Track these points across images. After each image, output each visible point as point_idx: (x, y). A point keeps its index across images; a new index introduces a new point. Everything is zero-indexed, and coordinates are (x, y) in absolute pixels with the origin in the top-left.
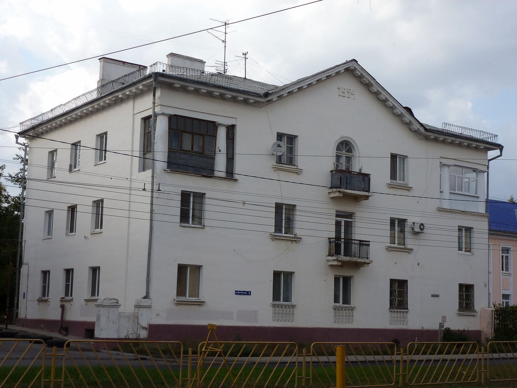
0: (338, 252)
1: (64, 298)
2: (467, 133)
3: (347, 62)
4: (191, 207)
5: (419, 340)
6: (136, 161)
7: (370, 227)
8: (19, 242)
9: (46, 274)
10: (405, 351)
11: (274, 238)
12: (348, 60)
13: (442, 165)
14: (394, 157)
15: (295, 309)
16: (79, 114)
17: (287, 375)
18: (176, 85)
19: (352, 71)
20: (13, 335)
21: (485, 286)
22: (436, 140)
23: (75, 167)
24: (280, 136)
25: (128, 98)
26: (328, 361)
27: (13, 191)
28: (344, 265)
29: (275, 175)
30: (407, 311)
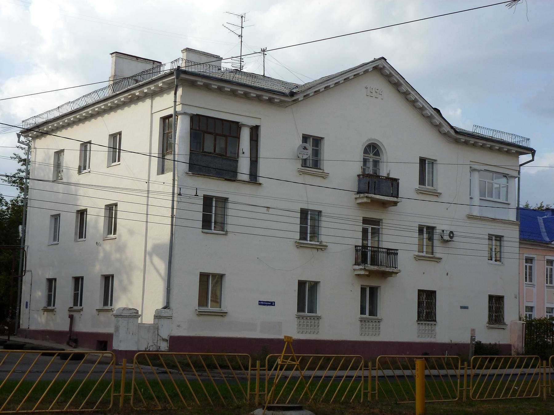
0: (364, 261)
1: (72, 308)
2: (498, 136)
3: (375, 60)
4: (214, 212)
5: (449, 354)
6: (155, 161)
7: (398, 234)
8: (22, 247)
9: (51, 282)
10: (469, 366)
11: (299, 246)
12: (377, 58)
13: (473, 170)
14: (423, 161)
15: (321, 321)
16: (90, 112)
17: (352, 390)
18: (199, 83)
19: (380, 69)
20: (21, 347)
21: (516, 297)
22: (466, 143)
23: (85, 169)
24: (305, 138)
25: (145, 96)
26: (383, 375)
27: (12, 193)
28: (371, 274)
29: (300, 179)
30: (435, 323)
